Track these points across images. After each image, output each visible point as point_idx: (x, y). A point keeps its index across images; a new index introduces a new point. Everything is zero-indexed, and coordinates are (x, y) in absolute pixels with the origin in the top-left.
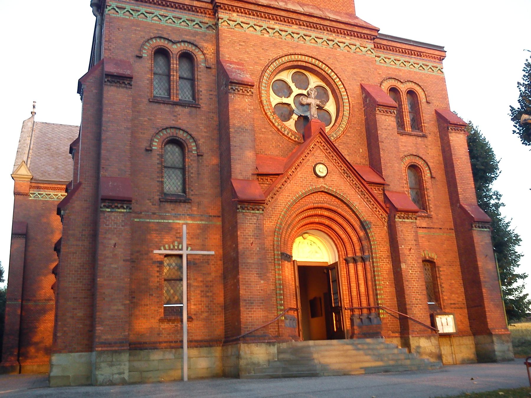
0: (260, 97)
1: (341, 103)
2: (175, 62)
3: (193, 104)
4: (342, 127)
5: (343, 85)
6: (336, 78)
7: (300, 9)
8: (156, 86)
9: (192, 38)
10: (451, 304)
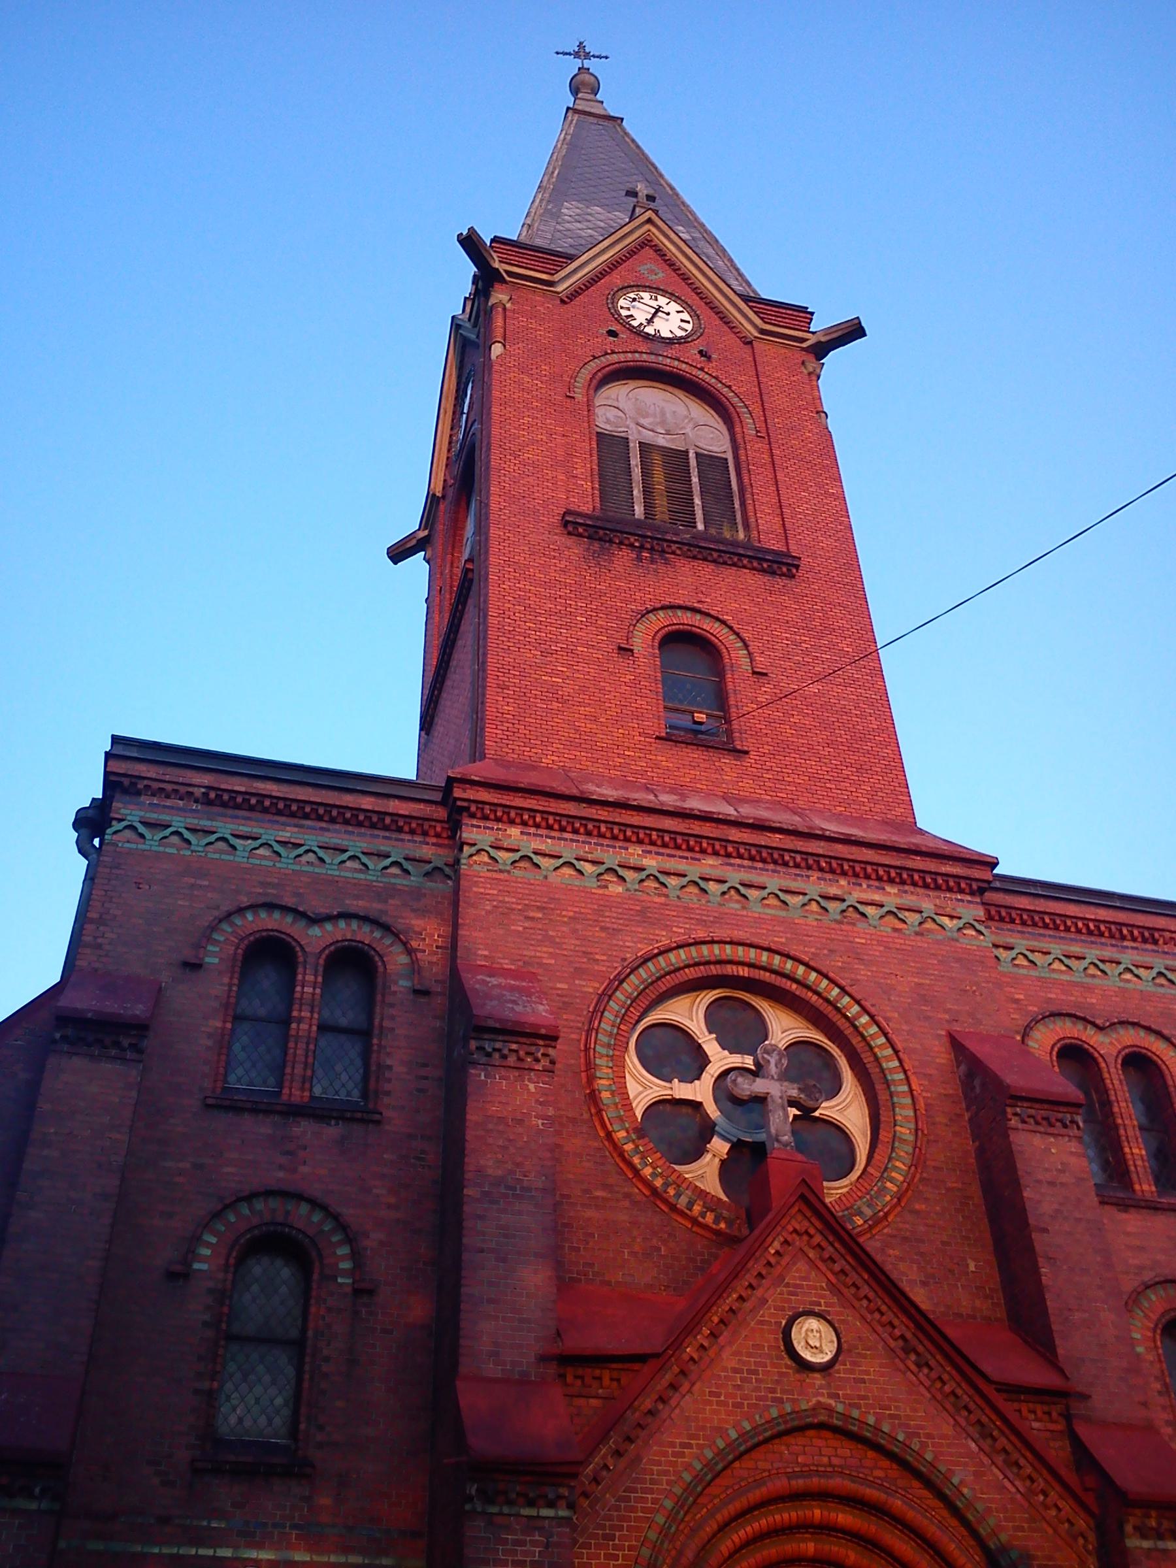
0: (591, 1079)
1: (883, 1097)
2: (310, 978)
3: (360, 1114)
4: (892, 1180)
5: (886, 1035)
7: (729, 811)
8: (242, 1056)
9: (380, 906)
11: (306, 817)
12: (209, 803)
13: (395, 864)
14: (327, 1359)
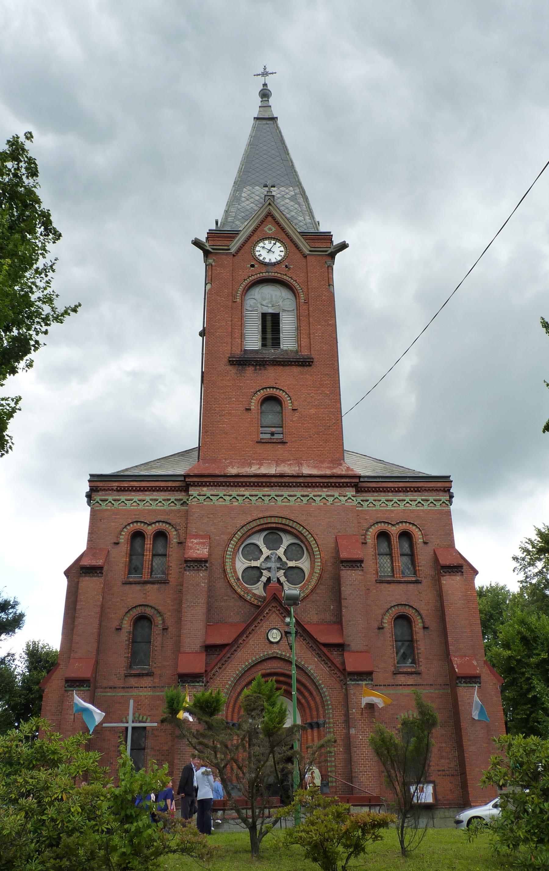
6: (308, 535)
9: (166, 517)
10: (438, 771)
11: (146, 491)
12: (118, 491)
13: (172, 502)
14: (156, 646)
